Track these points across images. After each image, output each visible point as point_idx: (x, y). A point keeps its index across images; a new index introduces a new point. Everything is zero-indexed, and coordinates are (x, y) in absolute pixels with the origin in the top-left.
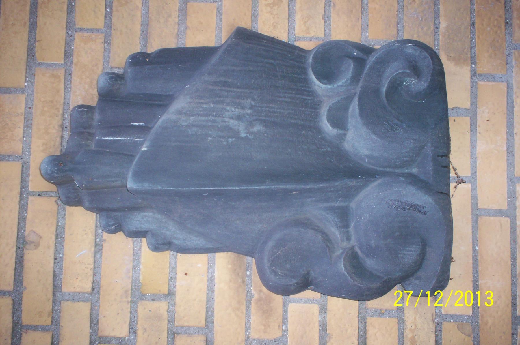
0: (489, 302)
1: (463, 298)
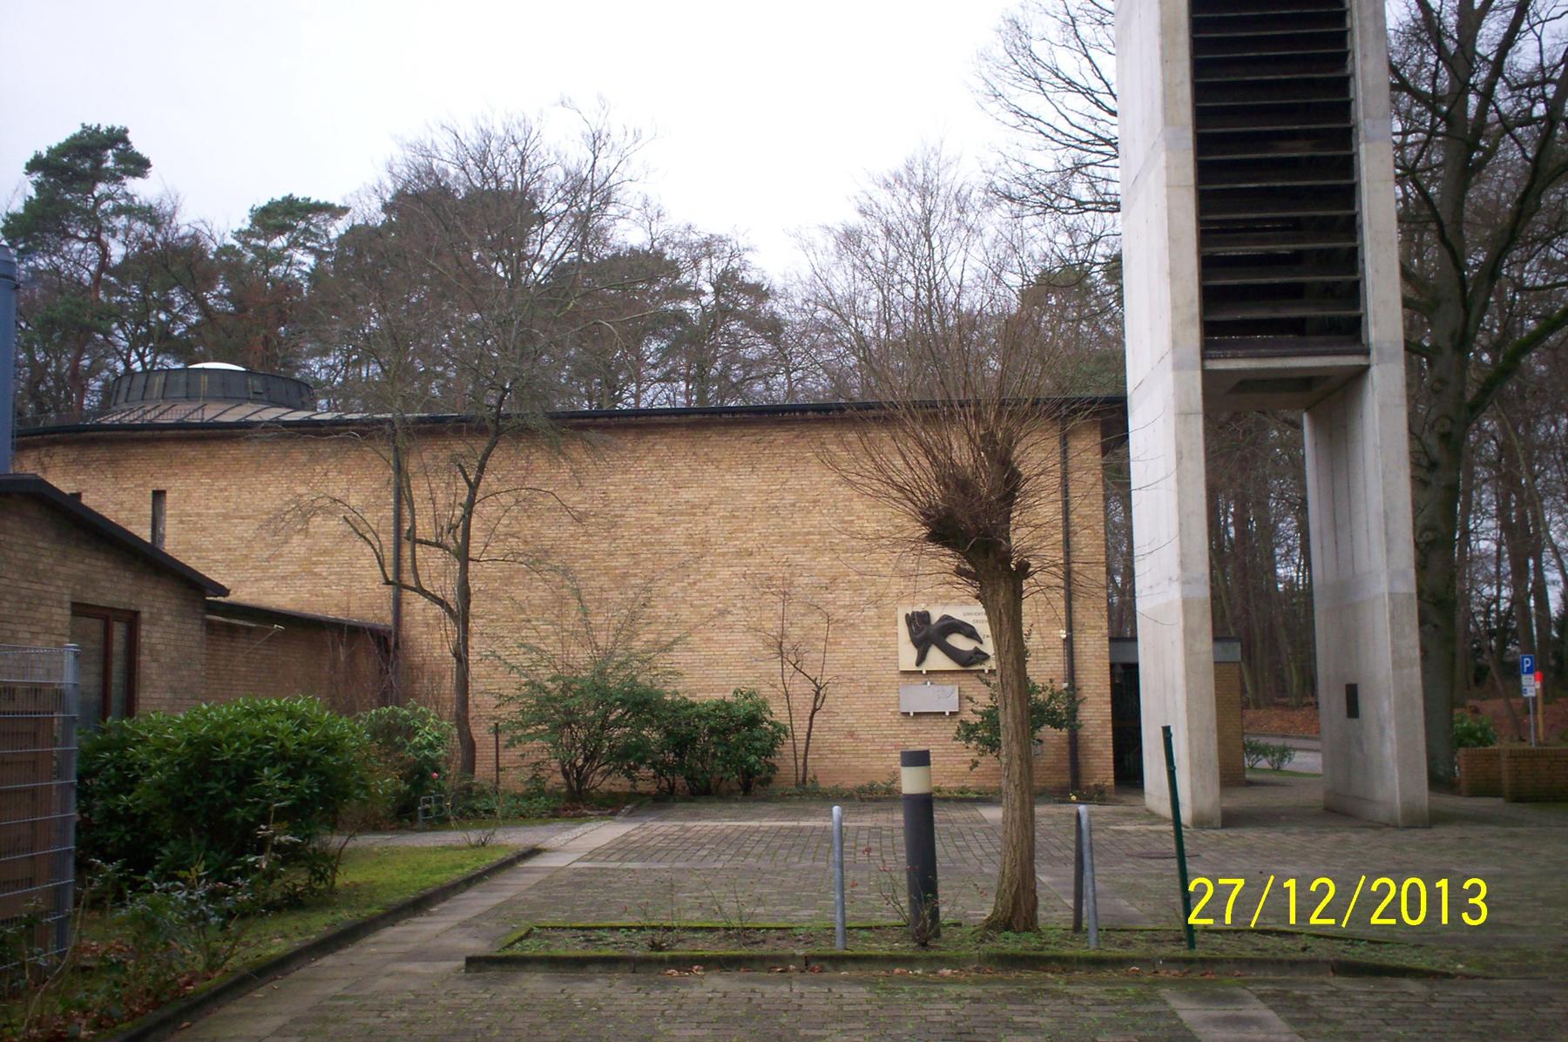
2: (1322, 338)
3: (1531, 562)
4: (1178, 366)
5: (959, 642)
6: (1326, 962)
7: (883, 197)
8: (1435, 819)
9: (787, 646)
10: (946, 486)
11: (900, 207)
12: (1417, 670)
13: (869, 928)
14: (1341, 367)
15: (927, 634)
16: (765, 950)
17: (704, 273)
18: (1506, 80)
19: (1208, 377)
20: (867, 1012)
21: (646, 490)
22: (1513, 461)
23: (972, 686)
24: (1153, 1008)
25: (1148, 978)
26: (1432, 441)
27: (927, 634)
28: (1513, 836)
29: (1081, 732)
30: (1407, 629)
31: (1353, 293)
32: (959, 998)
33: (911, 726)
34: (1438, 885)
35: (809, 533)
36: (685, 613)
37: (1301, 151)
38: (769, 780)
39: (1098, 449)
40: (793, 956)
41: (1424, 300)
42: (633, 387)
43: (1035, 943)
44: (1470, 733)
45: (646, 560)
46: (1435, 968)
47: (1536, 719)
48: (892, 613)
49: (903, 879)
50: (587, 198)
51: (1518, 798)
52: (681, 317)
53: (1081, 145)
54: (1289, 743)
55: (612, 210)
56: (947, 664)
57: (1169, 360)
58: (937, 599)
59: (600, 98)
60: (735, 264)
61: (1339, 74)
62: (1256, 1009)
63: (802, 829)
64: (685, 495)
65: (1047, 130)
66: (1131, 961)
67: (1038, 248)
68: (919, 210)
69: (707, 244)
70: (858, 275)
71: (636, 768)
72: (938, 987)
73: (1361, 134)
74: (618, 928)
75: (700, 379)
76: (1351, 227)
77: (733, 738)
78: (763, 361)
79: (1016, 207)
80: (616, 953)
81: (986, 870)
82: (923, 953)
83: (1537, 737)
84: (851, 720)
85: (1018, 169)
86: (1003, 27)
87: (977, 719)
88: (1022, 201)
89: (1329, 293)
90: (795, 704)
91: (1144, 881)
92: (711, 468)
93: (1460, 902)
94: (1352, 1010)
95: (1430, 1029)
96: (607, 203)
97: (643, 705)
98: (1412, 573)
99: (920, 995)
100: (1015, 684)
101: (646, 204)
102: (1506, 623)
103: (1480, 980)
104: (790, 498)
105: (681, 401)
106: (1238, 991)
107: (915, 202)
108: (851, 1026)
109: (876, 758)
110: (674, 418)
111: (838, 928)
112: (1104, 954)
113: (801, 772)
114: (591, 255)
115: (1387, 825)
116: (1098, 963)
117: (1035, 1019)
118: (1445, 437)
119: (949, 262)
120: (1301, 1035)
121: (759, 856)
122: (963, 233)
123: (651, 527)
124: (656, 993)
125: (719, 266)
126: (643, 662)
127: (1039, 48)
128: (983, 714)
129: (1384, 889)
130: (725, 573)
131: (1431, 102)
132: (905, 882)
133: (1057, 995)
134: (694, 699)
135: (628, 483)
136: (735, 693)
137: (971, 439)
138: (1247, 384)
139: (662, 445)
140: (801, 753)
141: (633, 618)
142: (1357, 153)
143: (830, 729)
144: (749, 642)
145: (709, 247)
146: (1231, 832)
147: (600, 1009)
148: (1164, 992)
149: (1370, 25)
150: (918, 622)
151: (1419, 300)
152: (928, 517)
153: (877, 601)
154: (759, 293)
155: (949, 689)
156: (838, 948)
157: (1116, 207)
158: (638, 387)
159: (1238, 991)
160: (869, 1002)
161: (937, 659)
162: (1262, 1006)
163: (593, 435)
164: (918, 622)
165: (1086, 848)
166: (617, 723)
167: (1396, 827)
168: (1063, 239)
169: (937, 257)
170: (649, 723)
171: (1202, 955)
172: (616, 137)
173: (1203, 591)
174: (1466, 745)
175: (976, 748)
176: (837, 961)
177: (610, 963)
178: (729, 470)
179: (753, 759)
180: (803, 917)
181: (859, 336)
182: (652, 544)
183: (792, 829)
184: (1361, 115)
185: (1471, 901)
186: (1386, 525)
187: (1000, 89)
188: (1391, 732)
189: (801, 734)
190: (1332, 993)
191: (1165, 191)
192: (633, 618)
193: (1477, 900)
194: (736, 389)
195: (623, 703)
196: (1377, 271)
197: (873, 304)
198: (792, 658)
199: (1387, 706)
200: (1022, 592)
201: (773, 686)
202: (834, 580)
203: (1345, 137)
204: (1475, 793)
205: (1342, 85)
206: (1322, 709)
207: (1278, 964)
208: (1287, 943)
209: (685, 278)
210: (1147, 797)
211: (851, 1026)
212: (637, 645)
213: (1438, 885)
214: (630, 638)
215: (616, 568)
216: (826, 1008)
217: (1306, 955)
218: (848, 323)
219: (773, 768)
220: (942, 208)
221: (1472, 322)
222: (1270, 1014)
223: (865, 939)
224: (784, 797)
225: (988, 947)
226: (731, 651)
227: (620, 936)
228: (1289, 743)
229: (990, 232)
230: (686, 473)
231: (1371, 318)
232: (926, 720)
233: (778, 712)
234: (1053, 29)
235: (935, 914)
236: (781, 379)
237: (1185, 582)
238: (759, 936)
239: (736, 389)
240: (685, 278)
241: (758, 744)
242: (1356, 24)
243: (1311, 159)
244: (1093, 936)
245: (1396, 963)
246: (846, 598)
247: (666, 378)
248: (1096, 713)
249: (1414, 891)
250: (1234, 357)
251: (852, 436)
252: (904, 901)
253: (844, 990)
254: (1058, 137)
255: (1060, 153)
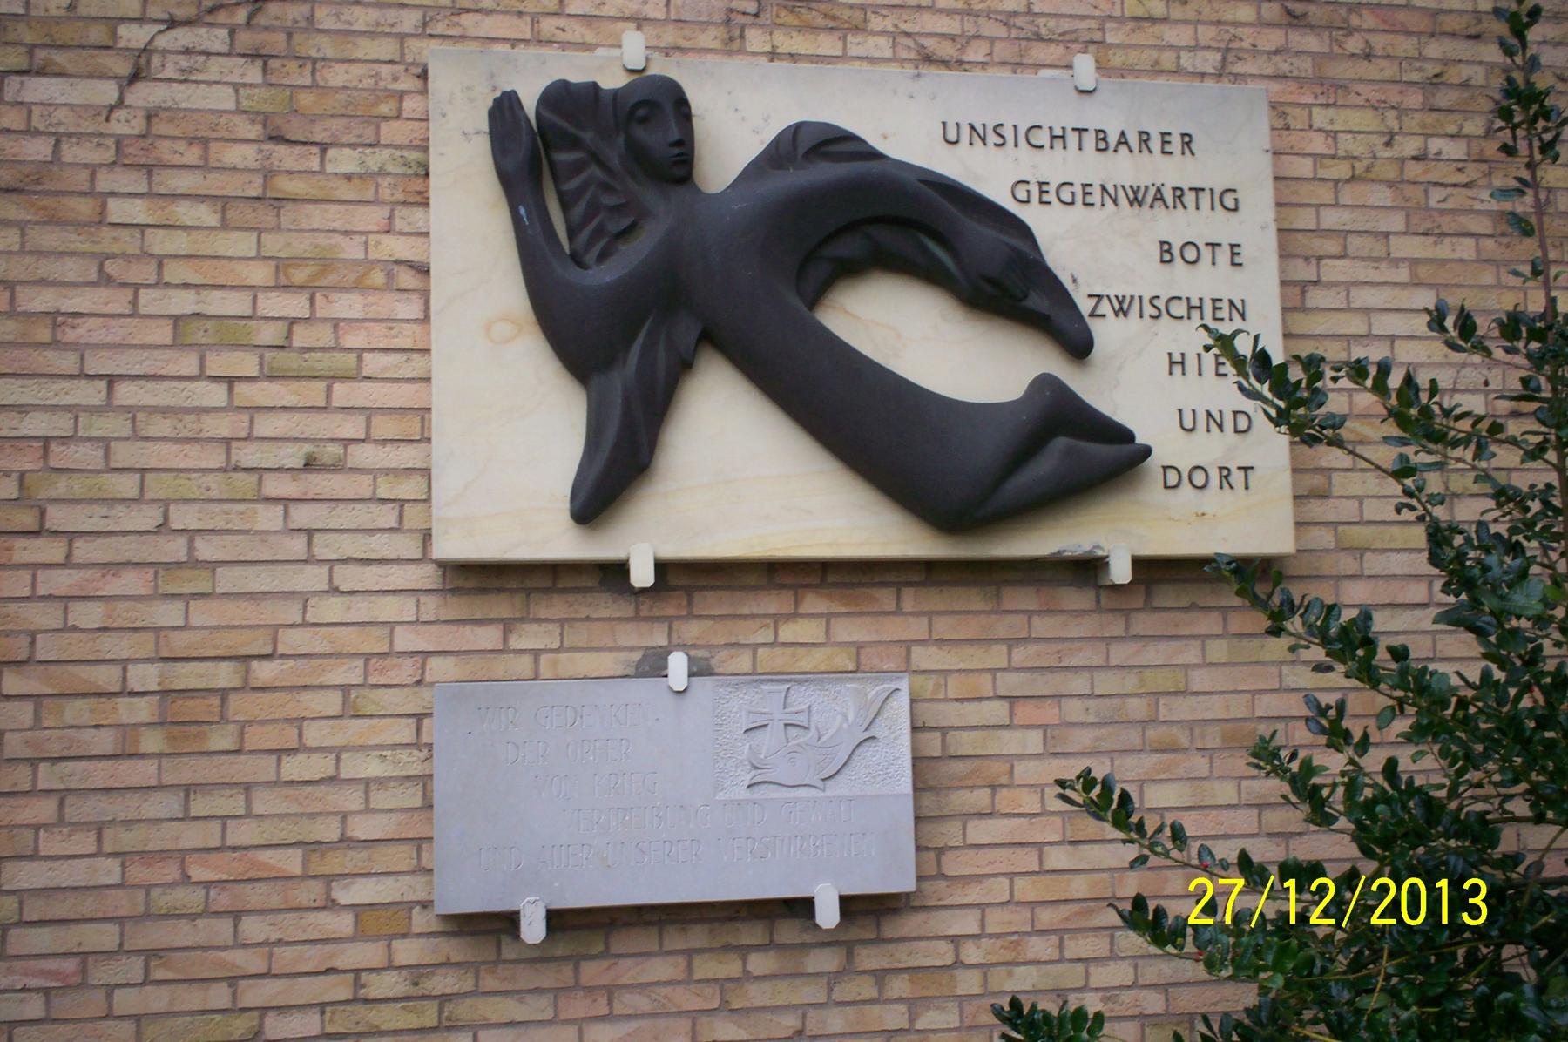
5: (908, 333)
23: (1042, 695)
34: (1438, 885)
56: (833, 514)
93: (1460, 901)
129: (1384, 889)
155: (835, 708)
161: (741, 474)
164: (590, 166)
185: (1471, 901)
193: (1477, 900)
213: (1438, 885)
232: (652, 968)
249: (1414, 893)
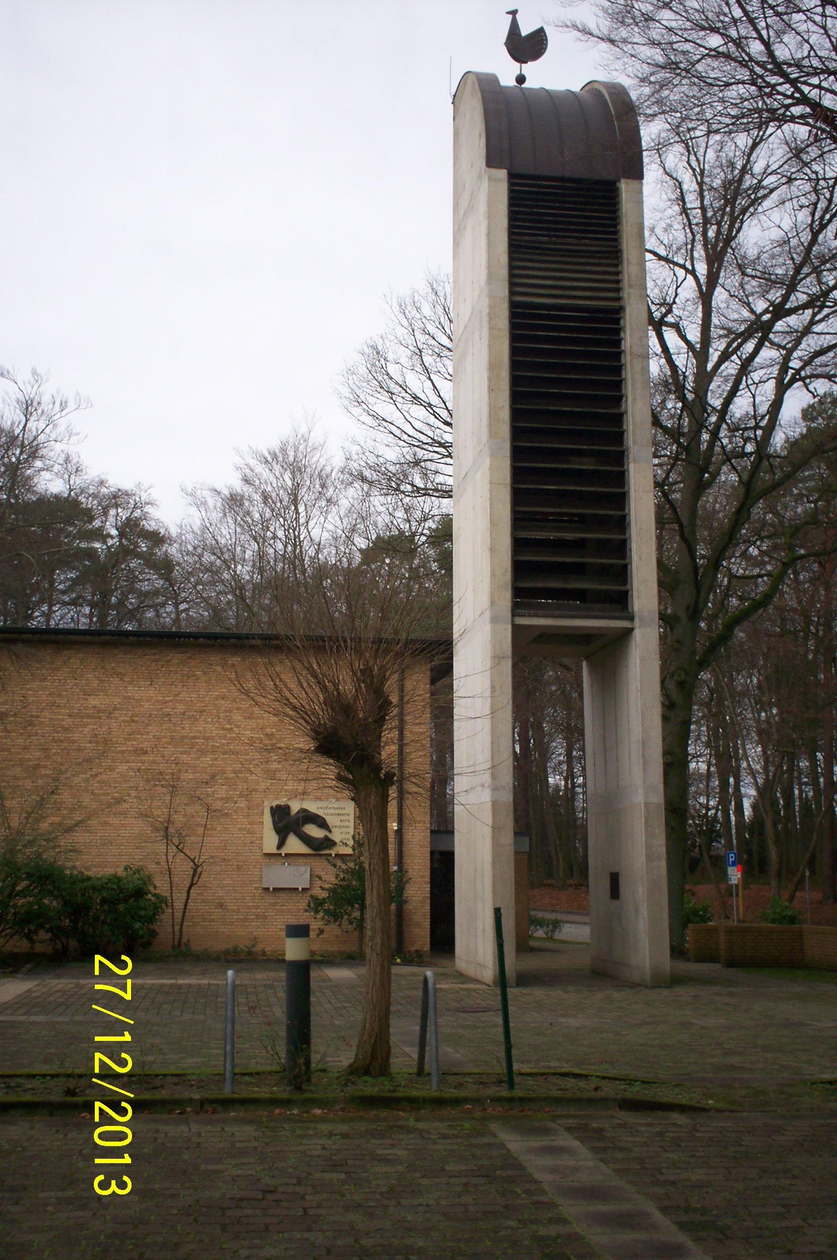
0: (104, 1185)
1: (114, 1122)
2: (599, 606)
3: (731, 780)
4: (494, 620)
5: (313, 831)
6: (614, 1100)
7: (260, 469)
8: (675, 980)
9: (172, 830)
10: (333, 709)
11: (275, 480)
12: (663, 863)
13: (250, 1074)
14: (613, 628)
15: (287, 822)
16: (162, 1094)
17: (111, 520)
18: (727, 424)
19: (517, 630)
20: (255, 1148)
21: (60, 695)
22: (720, 703)
24: (485, 1140)
25: (478, 1114)
26: (672, 686)
27: (287, 822)
28: (732, 994)
29: (408, 907)
30: (657, 831)
31: (622, 573)
32: (330, 1135)
33: (270, 899)
35: (195, 737)
36: (86, 799)
37: (586, 465)
38: (149, 944)
39: (428, 681)
40: (191, 1100)
41: (667, 580)
42: (45, 608)
43: (388, 1086)
44: (695, 913)
45: (55, 754)
46: (693, 1103)
47: (737, 901)
48: (260, 805)
49: (282, 1032)
50: (18, 452)
51: (732, 963)
52: (91, 554)
53: (421, 445)
54: (559, 917)
55: (38, 464)
57: (487, 615)
58: (294, 795)
59: (34, 373)
60: (137, 513)
61: (615, 411)
62: (564, 1140)
63: (180, 986)
64: (94, 701)
65: (398, 432)
66: (466, 1100)
67: (382, 520)
68: (290, 483)
69: (115, 497)
70: (239, 530)
71: (36, 933)
72: (312, 1125)
73: (631, 456)
74: (33, 1076)
75: (101, 606)
76: (622, 523)
77: (121, 907)
78: (156, 593)
79: (366, 487)
80: (36, 1099)
81: (337, 1022)
82: (296, 1096)
83: (738, 914)
84: (221, 893)
85: (372, 460)
86: (367, 350)
87: (325, 894)
88: (371, 483)
89: (603, 572)
90: (175, 879)
91: (461, 1031)
92: (116, 681)
94: (638, 1139)
95: (698, 1154)
96: (35, 457)
97: (46, 878)
98: (661, 787)
99: (298, 1132)
100: (380, 872)
101: (67, 460)
102: (713, 826)
103: (727, 1113)
104: (181, 708)
105: (83, 623)
106: (552, 1125)
107: (287, 477)
108: (244, 1160)
109: (270, 930)
110: (88, 638)
111: (228, 1075)
112: (443, 1095)
113: (177, 937)
114: (16, 497)
115: (640, 985)
116: (440, 1102)
117: (395, 1151)
118: (681, 684)
119: (311, 524)
120: (602, 1160)
121: (147, 1010)
122: (324, 503)
123: (63, 727)
124: (73, 1134)
125: (124, 515)
126: (48, 840)
127: (392, 369)
128: (330, 890)
130: (123, 768)
131: (674, 434)
132: (283, 1034)
133: (409, 1131)
134: (89, 873)
135: (45, 688)
136: (126, 869)
137: (354, 674)
138: (545, 636)
139: (75, 660)
140: (178, 920)
141: (41, 803)
142: (628, 470)
143: (203, 901)
144: (140, 826)
145: (117, 499)
146: (525, 990)
147: (24, 1149)
148: (493, 1126)
149: (638, 376)
150: (280, 814)
151: (667, 582)
152: (317, 733)
153: (248, 794)
154: (157, 538)
155: (303, 869)
156: (227, 1091)
157: (447, 494)
158: (50, 607)
159: (552, 1125)
160: (256, 1139)
162: (569, 1137)
163: (19, 648)
164: (280, 814)
165: (431, 1006)
166: (23, 893)
167: (646, 986)
168: (400, 514)
169: (302, 521)
170: (50, 893)
171: (520, 1095)
172: (46, 406)
173: (507, 797)
174: (693, 922)
175: (323, 918)
176: (227, 1103)
177: (31, 1107)
178: (131, 683)
179: (137, 925)
180: (189, 1064)
181: (236, 577)
182: (61, 741)
183: (172, 985)
184: (631, 443)
186: (644, 750)
187: (362, 398)
188: (644, 912)
189: (179, 905)
190: (620, 1126)
191: (488, 486)
192: (41, 803)
194: (132, 615)
195: (29, 875)
196: (640, 558)
197: (249, 554)
198: (176, 841)
199: (641, 891)
200: (388, 796)
201: (158, 863)
202: (213, 776)
203: (620, 458)
204: (700, 960)
205: (618, 419)
206: (592, 890)
207: (577, 1101)
208: (582, 1084)
209: (97, 523)
210: (457, 960)
211: (244, 1160)
212: (44, 826)
214: (37, 820)
215: (30, 760)
216: (221, 1145)
217: (598, 1094)
218: (229, 568)
219: (153, 933)
220: (308, 483)
221: (701, 600)
222: (576, 1144)
223: (248, 1084)
224: (163, 959)
225: (350, 1090)
226: (123, 833)
227: (36, 1083)
228: (559, 917)
229: (344, 503)
230: (96, 683)
231: (635, 593)
232: (283, 895)
233: (161, 886)
234: (404, 355)
235: (308, 1063)
236: (169, 608)
237: (495, 789)
238: (158, 1082)
239: (132, 615)
240: (97, 523)
241: (142, 913)
242: (629, 376)
243: (594, 471)
244: (435, 1079)
245: (665, 1100)
246: (222, 792)
247: (74, 603)
248: (418, 891)
250: (537, 616)
251: (236, 660)
252: (282, 1048)
253: (235, 1129)
254: (405, 437)
255: (405, 450)
